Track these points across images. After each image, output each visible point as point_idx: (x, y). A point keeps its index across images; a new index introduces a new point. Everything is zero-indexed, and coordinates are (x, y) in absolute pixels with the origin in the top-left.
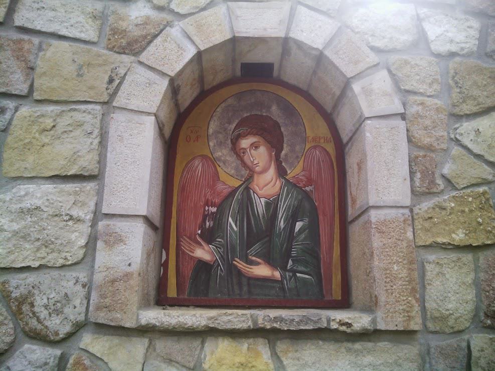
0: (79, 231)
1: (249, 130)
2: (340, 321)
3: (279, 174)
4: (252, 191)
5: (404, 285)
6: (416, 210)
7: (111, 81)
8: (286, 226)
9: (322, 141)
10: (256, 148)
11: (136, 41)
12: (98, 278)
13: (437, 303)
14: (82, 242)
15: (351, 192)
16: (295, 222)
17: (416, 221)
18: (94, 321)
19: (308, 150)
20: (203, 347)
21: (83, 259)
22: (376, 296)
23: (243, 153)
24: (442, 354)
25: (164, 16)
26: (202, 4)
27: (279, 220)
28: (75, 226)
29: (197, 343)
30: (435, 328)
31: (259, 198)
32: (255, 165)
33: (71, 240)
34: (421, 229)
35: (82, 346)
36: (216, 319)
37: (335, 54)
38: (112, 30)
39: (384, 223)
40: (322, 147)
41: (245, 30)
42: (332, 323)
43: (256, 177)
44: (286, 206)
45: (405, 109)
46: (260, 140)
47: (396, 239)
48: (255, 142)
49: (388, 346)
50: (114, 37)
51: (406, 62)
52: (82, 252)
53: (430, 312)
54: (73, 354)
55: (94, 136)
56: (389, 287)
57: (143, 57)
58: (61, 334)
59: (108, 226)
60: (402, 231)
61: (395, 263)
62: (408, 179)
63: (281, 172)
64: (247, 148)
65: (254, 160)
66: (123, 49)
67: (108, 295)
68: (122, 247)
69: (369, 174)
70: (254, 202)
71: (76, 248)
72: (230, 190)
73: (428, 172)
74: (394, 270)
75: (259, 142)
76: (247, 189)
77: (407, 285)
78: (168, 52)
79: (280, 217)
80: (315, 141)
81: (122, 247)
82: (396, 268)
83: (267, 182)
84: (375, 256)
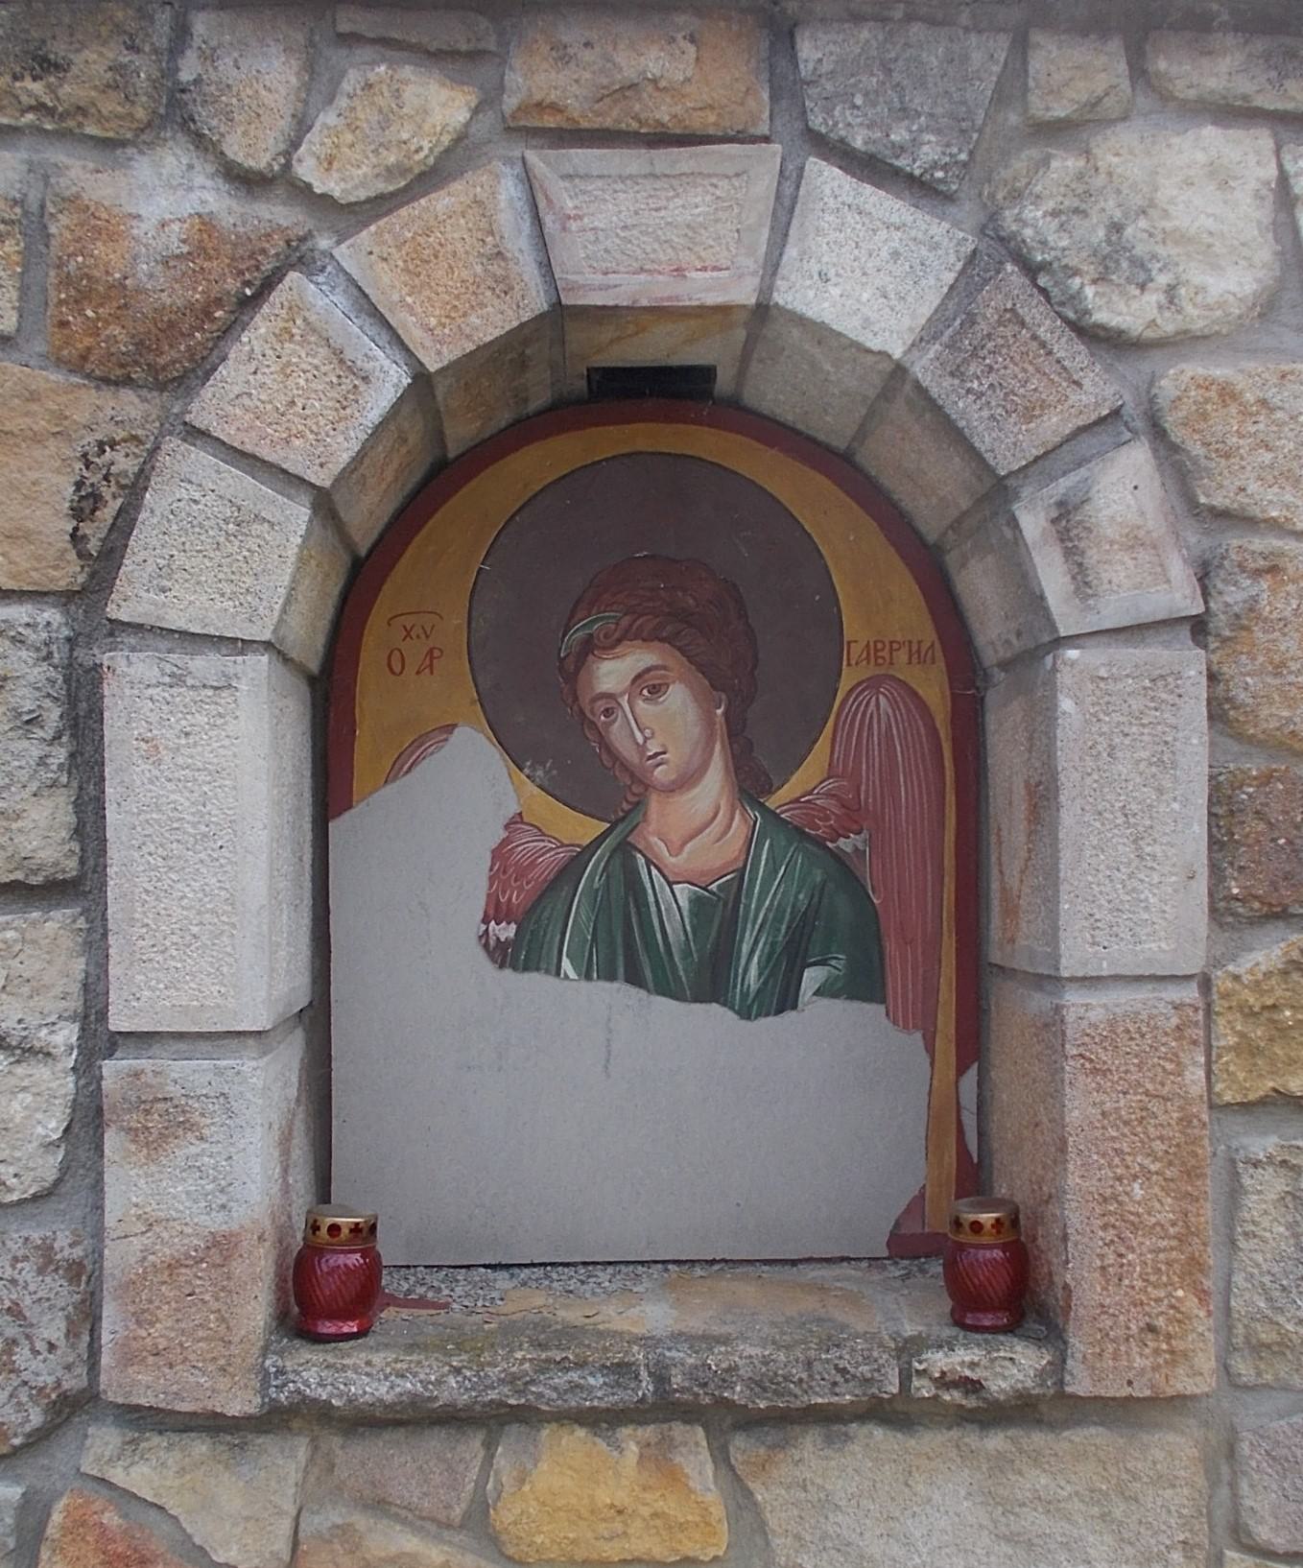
0: (34, 1090)
1: (625, 621)
2: (943, 1373)
3: (742, 790)
4: (641, 860)
5: (1164, 1250)
6: (1221, 981)
7: (86, 504)
8: (765, 983)
9: (902, 656)
10: (656, 690)
11: (170, 329)
12: (120, 1258)
13: (1270, 1299)
14: (53, 1126)
15: (1002, 881)
16: (797, 969)
17: (1221, 1021)
18: (120, 1400)
19: (851, 691)
20: (489, 1458)
21: (58, 1182)
22: (1066, 1287)
23: (607, 712)
24: (1274, 1459)
25: (278, 214)
26: (422, 155)
27: (743, 962)
28: (20, 1070)
29: (472, 1446)
30: (1259, 1374)
31: (670, 884)
32: (650, 758)
33: (11, 1120)
34: (1235, 1049)
35: (88, 1467)
36: (532, 1382)
37: (952, 374)
38: (67, 281)
39: (1112, 1033)
40: (903, 684)
41: (598, 279)
42: (916, 1383)
43: (654, 803)
44: (769, 909)
45: (1206, 594)
46: (670, 663)
47: (1147, 1093)
48: (648, 670)
49: (1098, 1441)
50: (81, 312)
51: (1228, 394)
52: (49, 1167)
53: (1246, 1326)
54: (62, 1494)
55: (48, 733)
56: (1111, 1259)
57: (206, 408)
58: (16, 1435)
59: (137, 1075)
60: (1169, 1066)
61: (1135, 1177)
62: (1203, 872)
63: (751, 784)
64: (622, 694)
65: (646, 739)
66: (122, 366)
67: (161, 1314)
68: (193, 1150)
69: (1066, 856)
70: (651, 899)
71: (31, 1148)
72: (563, 855)
73: (1273, 840)
74: (1131, 1200)
75: (664, 668)
76: (625, 850)
77: (1172, 1249)
78: (302, 382)
79: (745, 948)
80: (876, 658)
81: (193, 1150)
82: (1138, 1192)
83: (698, 822)
84: (1072, 1155)
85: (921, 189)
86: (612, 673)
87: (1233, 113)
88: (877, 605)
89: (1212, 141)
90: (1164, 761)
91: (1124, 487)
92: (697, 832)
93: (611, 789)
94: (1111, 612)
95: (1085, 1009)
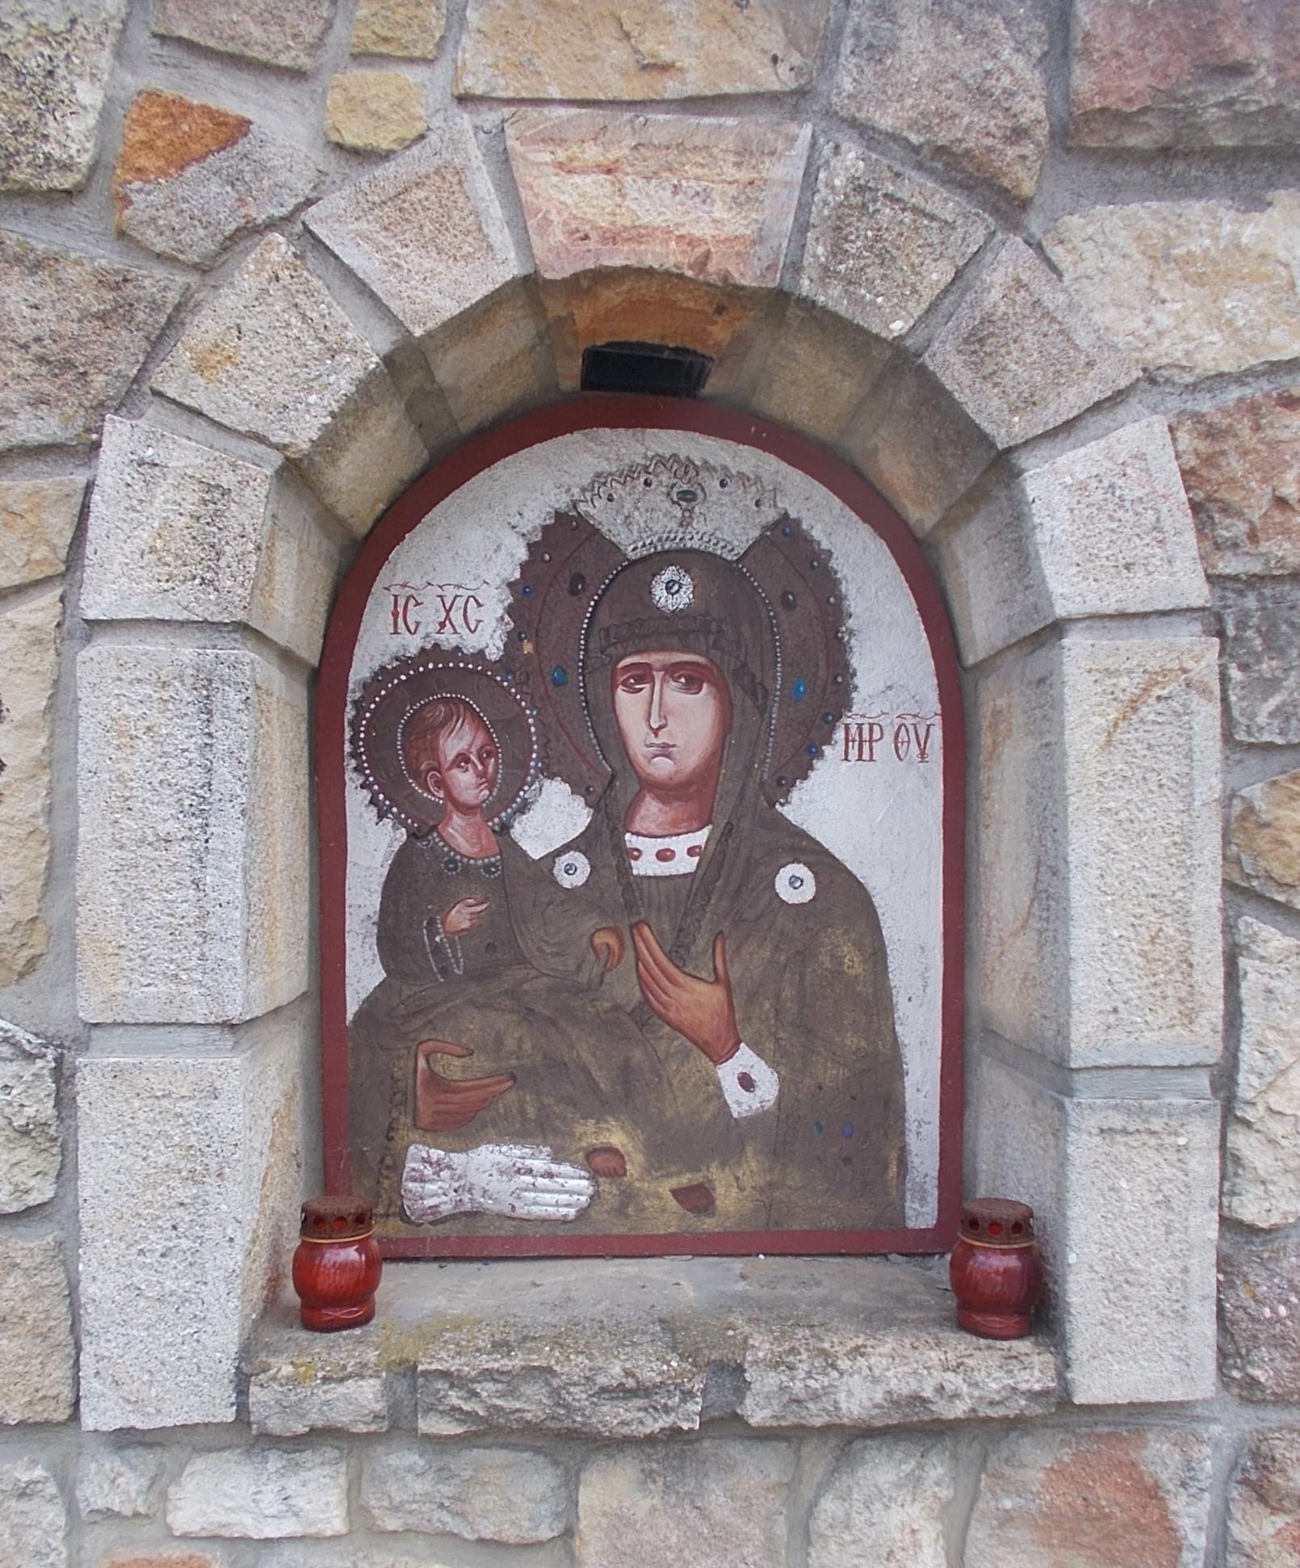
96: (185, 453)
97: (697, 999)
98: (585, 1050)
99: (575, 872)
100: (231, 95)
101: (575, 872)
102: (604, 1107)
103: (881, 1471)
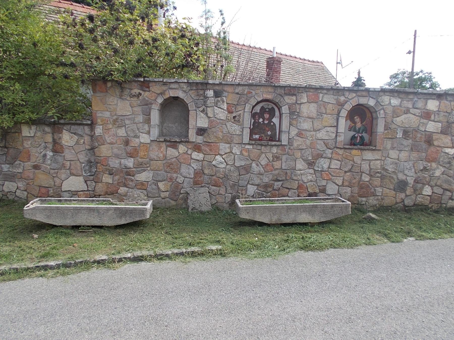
12: (338, 141)
25: (347, 99)
63: (361, 123)
85: (374, 99)
86: (355, 118)
87: (388, 95)
88: (368, 115)
89: (387, 97)
90: (383, 123)
91: (382, 112)
92: (359, 125)
93: (355, 123)
94: (381, 117)
95: (378, 133)
96: (249, 105)
97: (267, 129)
98: (262, 131)
99: (262, 123)
100: (252, 91)
101: (262, 123)
102: (262, 134)
103: (274, 147)
